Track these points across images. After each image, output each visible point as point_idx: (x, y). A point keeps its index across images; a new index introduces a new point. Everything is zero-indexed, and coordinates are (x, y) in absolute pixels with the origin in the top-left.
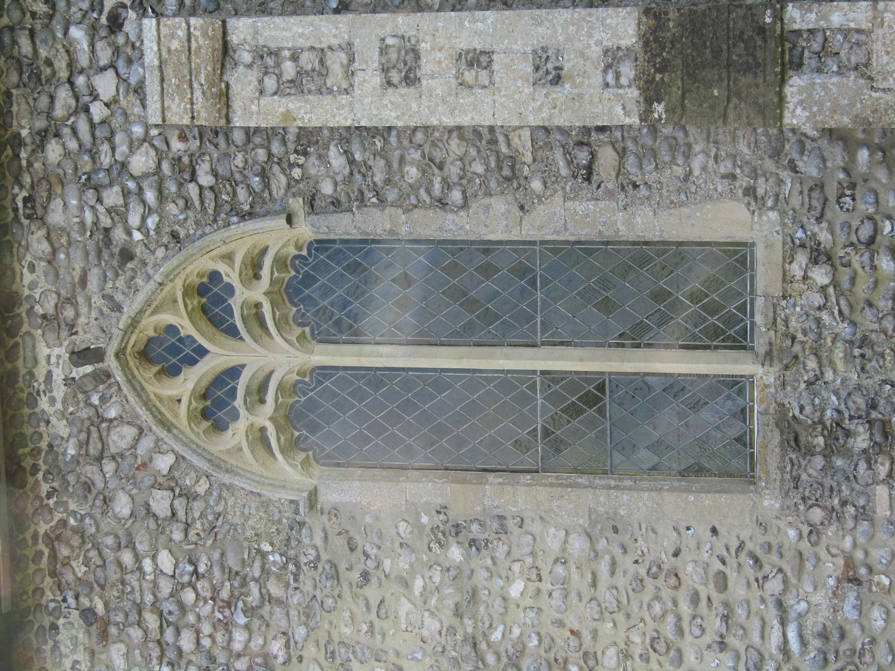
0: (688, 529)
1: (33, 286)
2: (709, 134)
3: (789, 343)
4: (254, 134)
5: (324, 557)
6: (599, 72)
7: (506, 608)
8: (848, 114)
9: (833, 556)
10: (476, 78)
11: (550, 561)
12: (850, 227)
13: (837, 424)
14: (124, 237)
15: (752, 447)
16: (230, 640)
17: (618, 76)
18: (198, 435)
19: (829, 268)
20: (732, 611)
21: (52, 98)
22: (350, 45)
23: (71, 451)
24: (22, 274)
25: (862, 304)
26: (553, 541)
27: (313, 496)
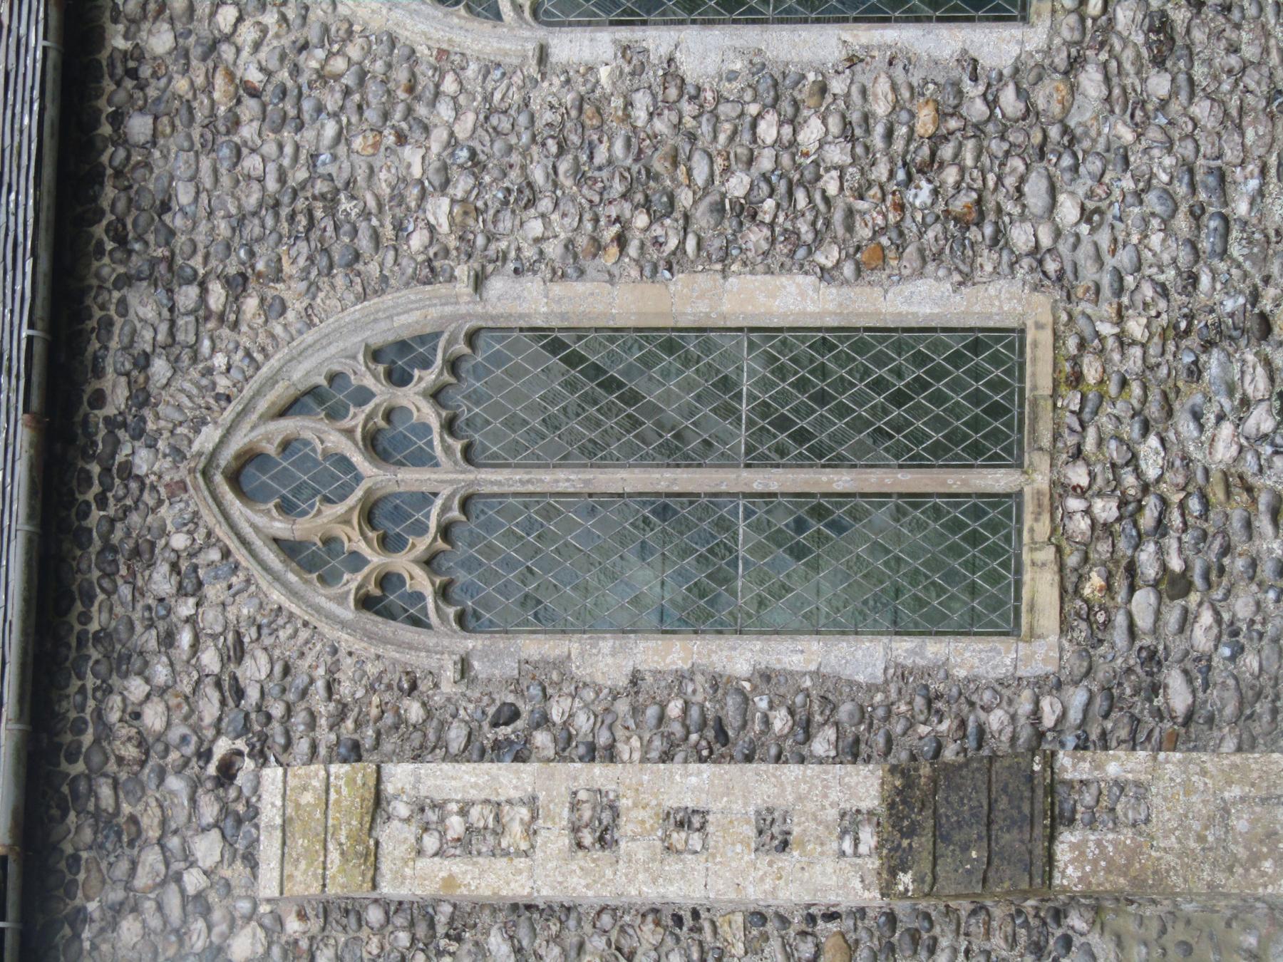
6: (834, 837)
8: (1125, 875)
17: (857, 842)
21: (134, 865)
22: (534, 799)
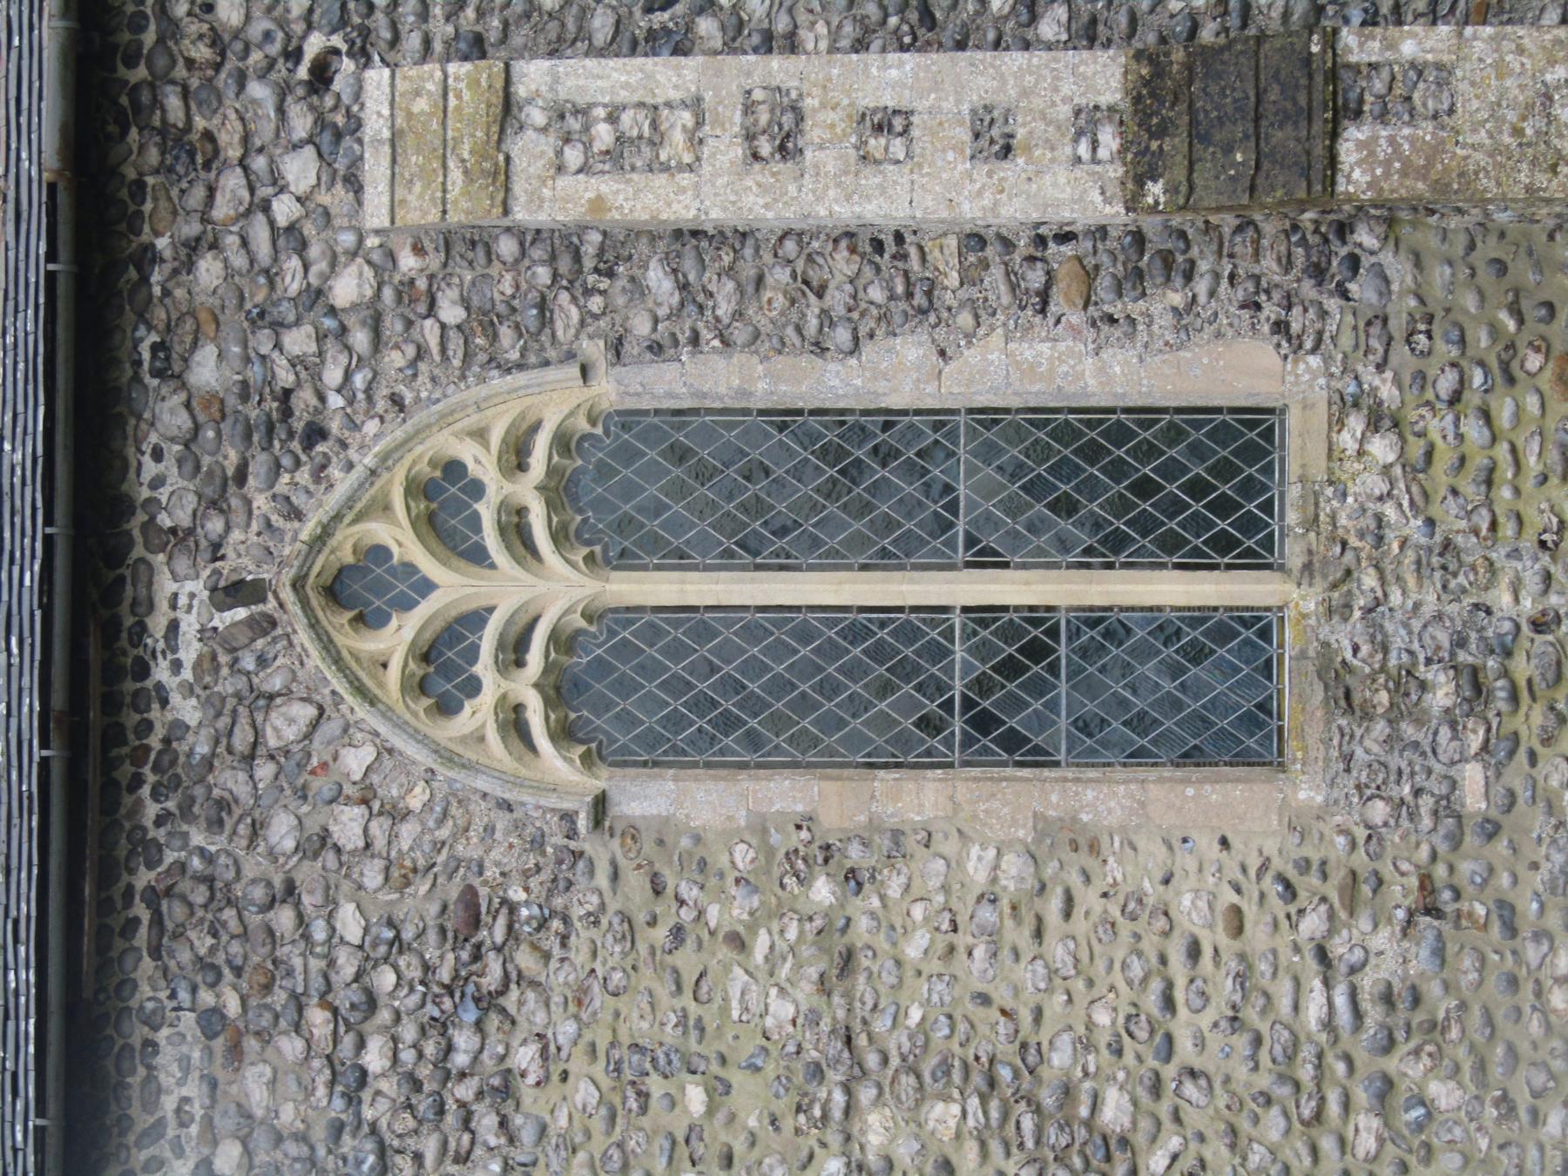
0: (1185, 840)
1: (158, 482)
2: (1221, 245)
3: (1338, 549)
4: (533, 243)
5: (613, 906)
7: (901, 979)
8: (1424, 178)
9: (1403, 874)
10: (886, 149)
11: (971, 899)
12: (1424, 378)
13: (1409, 673)
14: (314, 401)
15: (1280, 718)
16: (450, 1048)
18: (415, 715)
19: (1395, 438)
20: (1250, 967)
21: (211, 191)
22: (699, 100)
23: (203, 749)
24: (140, 464)
25: (1443, 491)
26: (977, 868)
27: (600, 804)
